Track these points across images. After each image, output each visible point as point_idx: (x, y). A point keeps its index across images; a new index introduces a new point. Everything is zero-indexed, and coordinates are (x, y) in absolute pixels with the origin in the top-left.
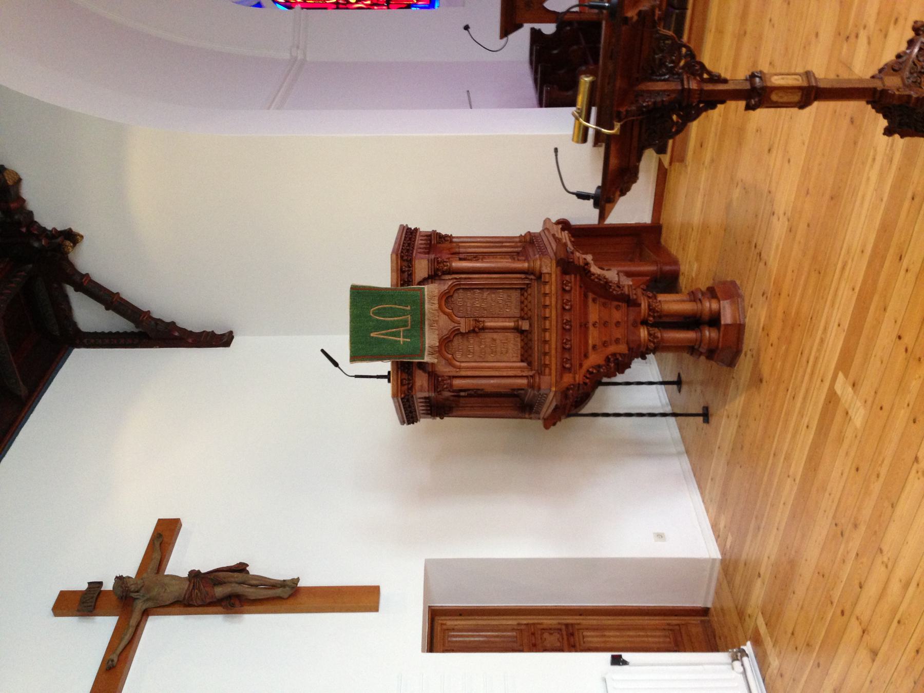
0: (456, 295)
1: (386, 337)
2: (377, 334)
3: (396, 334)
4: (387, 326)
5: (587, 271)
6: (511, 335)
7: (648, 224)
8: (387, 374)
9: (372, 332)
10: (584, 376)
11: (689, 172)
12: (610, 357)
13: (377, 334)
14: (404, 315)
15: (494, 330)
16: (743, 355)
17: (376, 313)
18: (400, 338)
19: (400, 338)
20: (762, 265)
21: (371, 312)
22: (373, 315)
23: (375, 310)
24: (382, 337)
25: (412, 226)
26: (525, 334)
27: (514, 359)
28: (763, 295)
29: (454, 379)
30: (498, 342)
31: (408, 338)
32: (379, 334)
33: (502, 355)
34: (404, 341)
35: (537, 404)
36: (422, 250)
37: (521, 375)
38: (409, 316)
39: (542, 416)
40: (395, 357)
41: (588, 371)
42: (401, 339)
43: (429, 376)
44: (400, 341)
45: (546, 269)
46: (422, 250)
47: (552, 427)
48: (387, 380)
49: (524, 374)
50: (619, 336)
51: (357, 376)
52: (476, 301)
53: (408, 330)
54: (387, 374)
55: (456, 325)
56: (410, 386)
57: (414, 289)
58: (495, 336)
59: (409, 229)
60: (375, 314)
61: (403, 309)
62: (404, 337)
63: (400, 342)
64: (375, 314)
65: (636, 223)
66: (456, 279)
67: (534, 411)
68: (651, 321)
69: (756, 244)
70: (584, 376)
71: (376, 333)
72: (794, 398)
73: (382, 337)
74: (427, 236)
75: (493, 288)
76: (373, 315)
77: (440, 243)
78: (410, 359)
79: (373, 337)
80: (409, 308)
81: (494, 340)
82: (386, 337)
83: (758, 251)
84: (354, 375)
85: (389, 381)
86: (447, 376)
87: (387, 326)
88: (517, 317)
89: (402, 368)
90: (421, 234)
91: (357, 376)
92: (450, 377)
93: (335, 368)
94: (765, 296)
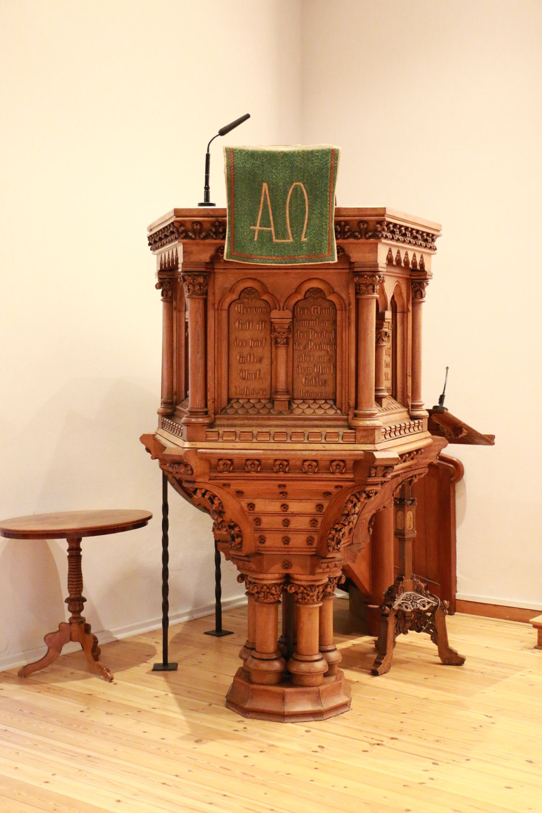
0: (326, 304)
1: (262, 205)
2: (265, 192)
3: (265, 223)
4: (278, 207)
5: (358, 496)
6: (266, 384)
7: (455, 596)
8: (211, 201)
9: (268, 184)
10: (206, 491)
11: (522, 652)
12: (237, 529)
13: (265, 192)
14: (293, 234)
15: (273, 362)
16: (241, 718)
17: (297, 191)
18: (260, 226)
19: (260, 226)
20: (366, 746)
21: (297, 183)
22: (293, 187)
23: (301, 189)
24: (262, 200)
25: (437, 243)
26: (269, 406)
27: (233, 390)
28: (321, 747)
29: (202, 302)
30: (258, 366)
31: (258, 238)
32: (265, 195)
33: (239, 372)
34: (254, 231)
35: (172, 423)
36: (394, 255)
37: (209, 398)
38: (291, 240)
39: (161, 431)
40: (232, 215)
41: (215, 496)
42: (258, 228)
43: (206, 263)
44: (255, 225)
45: (362, 436)
46: (394, 255)
47: (143, 447)
48: (203, 201)
49: (209, 403)
50: (268, 543)
51: (208, 156)
52: (318, 335)
53: (271, 240)
54: (211, 201)
55: (282, 305)
56: (191, 234)
57: (330, 244)
58: (266, 362)
59: (433, 237)
60: (297, 191)
61: (302, 231)
62: (261, 233)
63: (253, 226)
64: (296, 189)
65: (456, 577)
66: (350, 304)
67: (165, 419)
68: (290, 589)
69: (396, 739)
70: (206, 491)
71: (267, 192)
72: (164, 784)
73: (262, 200)
74: (422, 265)
75: (173, 375)
76: (293, 187)
77: (412, 284)
78: (228, 238)
79: (262, 186)
80: (304, 239)
81: (260, 360)
82: (262, 205)
83: (386, 741)
84: (210, 153)
85: (201, 204)
86: (207, 290)
87: (278, 207)
88: (293, 393)
89: (217, 223)
90: (425, 257)
91: (208, 156)
92: (206, 293)
93: (219, 130)
94: (319, 749)
